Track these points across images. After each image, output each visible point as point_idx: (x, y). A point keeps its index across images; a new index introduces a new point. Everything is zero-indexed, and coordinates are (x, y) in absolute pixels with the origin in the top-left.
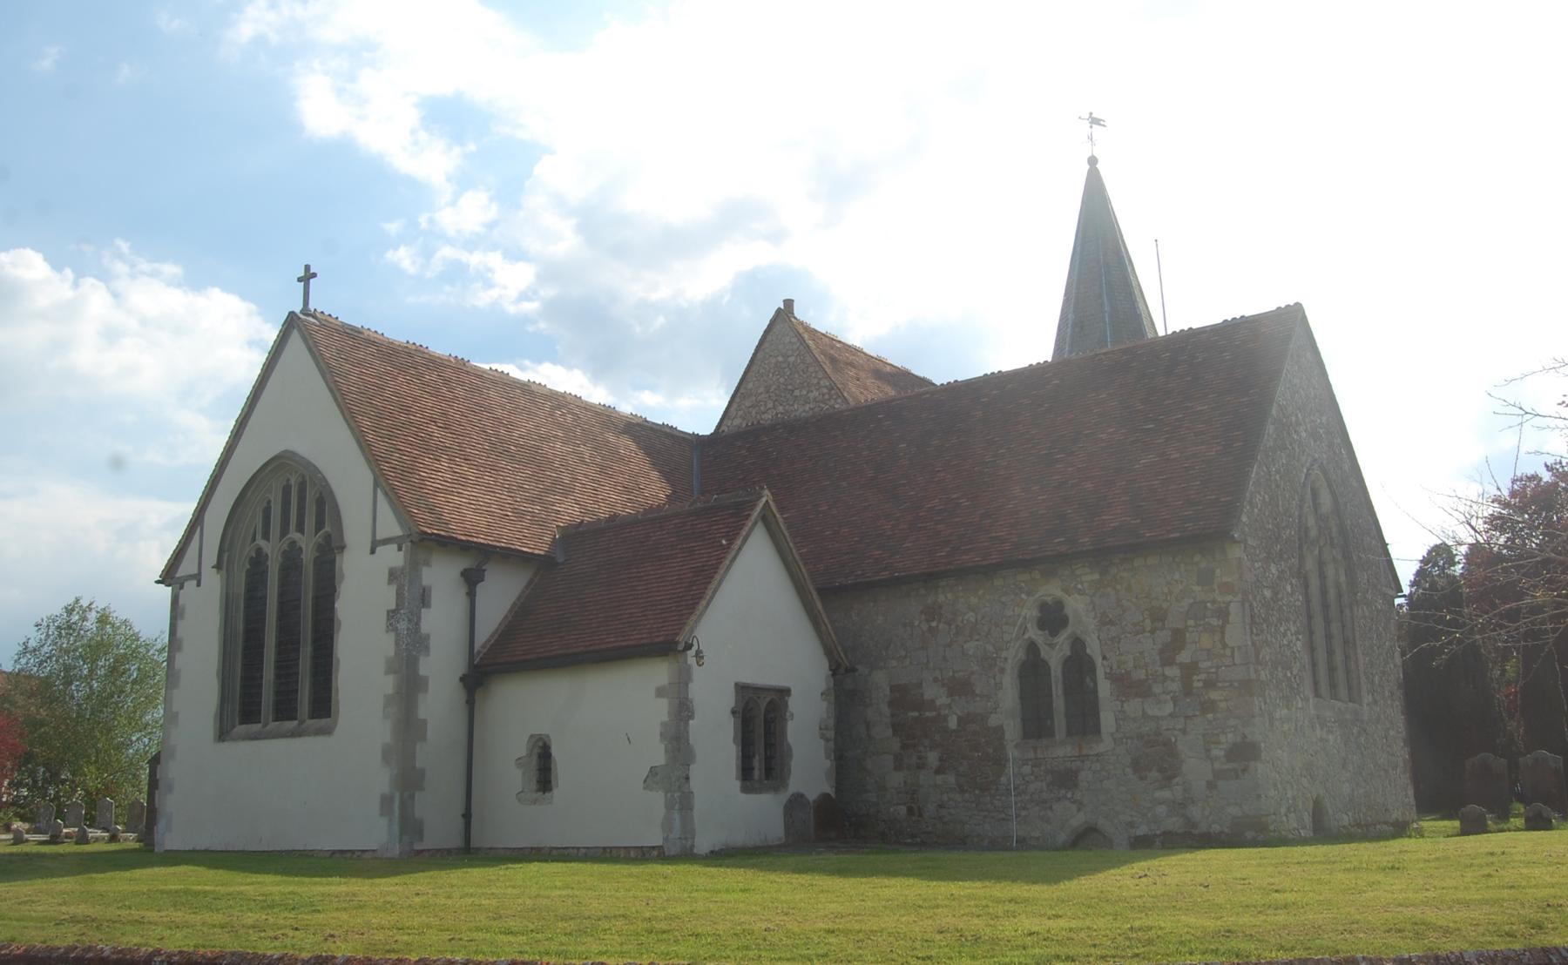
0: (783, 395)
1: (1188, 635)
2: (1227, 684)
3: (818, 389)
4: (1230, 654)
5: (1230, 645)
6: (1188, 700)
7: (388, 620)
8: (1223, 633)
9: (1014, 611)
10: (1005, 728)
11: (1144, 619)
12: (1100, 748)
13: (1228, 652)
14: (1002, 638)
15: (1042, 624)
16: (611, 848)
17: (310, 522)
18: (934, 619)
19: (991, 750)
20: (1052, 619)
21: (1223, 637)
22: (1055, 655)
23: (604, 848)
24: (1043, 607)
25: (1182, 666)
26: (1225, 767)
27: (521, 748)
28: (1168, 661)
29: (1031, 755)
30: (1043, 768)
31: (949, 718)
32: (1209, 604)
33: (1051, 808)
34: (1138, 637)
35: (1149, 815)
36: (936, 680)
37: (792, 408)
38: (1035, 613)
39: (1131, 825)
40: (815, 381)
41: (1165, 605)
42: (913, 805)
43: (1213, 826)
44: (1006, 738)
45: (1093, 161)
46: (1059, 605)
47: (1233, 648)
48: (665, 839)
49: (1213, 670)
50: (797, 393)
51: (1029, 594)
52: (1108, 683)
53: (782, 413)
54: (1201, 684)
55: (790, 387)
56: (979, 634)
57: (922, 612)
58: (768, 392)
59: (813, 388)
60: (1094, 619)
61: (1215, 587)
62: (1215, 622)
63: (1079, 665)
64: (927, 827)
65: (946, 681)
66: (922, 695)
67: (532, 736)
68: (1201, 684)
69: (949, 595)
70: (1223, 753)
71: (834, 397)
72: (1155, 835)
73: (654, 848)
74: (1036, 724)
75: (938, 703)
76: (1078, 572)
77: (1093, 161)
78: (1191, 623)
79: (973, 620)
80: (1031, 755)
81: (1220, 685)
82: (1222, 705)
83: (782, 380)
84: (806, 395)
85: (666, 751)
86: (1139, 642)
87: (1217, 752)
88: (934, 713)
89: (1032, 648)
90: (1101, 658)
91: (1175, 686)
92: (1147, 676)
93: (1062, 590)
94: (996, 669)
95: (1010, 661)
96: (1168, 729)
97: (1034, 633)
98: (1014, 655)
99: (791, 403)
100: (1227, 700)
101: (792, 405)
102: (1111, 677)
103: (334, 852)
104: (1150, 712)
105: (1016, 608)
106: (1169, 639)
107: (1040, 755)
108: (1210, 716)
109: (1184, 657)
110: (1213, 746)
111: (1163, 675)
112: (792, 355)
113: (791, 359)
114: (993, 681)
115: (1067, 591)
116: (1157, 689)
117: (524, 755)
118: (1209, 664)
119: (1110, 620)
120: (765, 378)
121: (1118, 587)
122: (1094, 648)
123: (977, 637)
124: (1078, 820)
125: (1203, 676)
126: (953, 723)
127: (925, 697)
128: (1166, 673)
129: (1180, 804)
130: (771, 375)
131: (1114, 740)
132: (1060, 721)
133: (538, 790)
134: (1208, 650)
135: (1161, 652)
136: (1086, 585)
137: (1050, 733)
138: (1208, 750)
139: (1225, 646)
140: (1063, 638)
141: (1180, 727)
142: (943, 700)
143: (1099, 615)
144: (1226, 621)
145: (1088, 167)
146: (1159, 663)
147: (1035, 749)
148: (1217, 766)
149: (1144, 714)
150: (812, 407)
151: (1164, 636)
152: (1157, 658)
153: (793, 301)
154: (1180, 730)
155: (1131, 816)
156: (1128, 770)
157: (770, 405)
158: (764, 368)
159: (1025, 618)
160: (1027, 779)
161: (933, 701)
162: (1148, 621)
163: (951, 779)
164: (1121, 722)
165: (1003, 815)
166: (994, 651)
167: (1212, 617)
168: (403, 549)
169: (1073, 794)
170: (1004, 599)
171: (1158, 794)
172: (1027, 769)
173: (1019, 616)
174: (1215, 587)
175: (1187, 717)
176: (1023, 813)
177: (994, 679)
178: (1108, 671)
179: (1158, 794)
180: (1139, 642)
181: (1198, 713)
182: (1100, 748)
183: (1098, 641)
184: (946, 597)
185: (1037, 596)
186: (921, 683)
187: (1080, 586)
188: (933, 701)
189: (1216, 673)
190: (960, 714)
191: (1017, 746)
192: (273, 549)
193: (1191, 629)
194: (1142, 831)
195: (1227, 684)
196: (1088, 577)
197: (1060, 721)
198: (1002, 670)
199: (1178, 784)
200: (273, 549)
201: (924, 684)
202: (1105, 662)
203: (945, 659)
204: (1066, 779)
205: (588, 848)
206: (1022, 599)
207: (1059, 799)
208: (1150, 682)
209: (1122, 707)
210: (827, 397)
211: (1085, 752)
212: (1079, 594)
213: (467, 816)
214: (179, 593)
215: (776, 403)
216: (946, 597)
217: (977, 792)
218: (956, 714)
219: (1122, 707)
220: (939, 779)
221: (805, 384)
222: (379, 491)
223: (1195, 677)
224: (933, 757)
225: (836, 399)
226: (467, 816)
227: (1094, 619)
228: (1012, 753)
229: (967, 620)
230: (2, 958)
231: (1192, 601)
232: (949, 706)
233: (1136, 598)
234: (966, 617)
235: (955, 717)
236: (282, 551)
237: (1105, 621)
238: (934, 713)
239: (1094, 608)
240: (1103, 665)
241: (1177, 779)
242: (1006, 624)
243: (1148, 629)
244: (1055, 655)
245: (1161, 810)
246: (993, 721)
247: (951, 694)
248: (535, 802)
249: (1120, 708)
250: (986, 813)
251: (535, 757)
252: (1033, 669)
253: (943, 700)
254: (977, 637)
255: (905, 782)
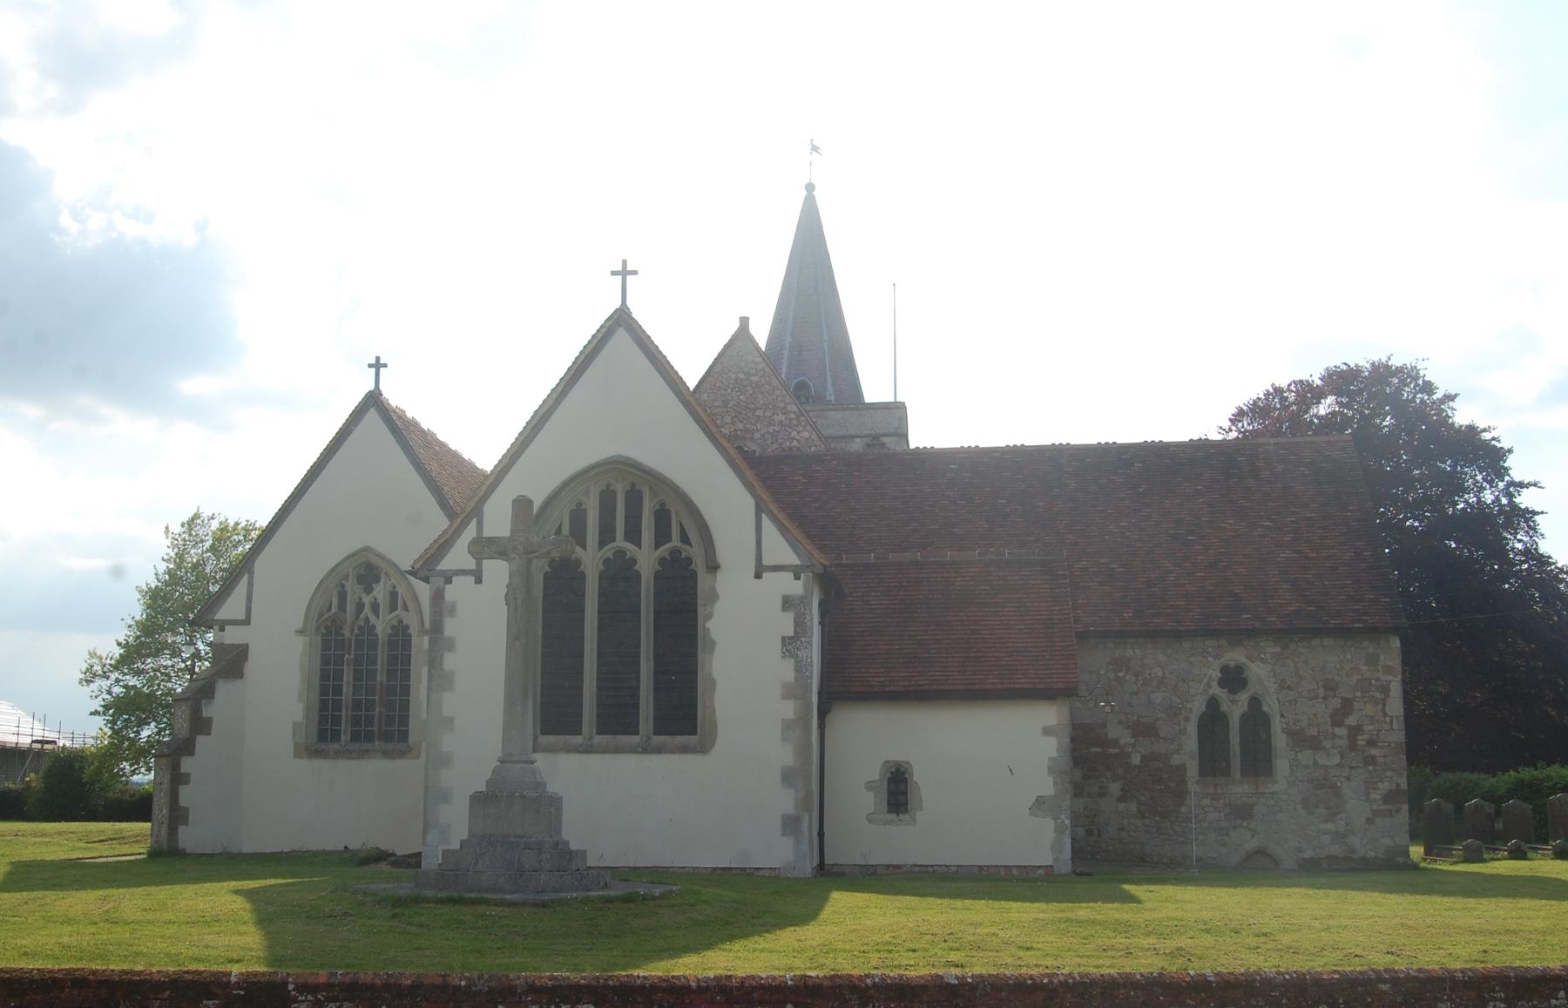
0: (744, 412)
1: (1355, 703)
2: (1386, 744)
3: (785, 413)
4: (1389, 721)
5: (1389, 713)
6: (1353, 754)
7: (784, 645)
8: (1384, 705)
9: (1200, 671)
10: (1187, 766)
11: (1319, 688)
12: (1276, 788)
13: (1388, 720)
14: (1189, 692)
15: (1222, 683)
16: (988, 866)
17: (647, 535)
18: (1121, 671)
19: (1173, 785)
20: (1233, 679)
21: (1384, 708)
22: (1235, 709)
23: (981, 867)
24: (1225, 670)
25: (1350, 728)
26: (1383, 807)
27: (875, 773)
28: (1337, 723)
29: (1211, 790)
30: (1222, 801)
31: (1132, 756)
32: (1373, 681)
33: (1228, 834)
34: (1313, 701)
35: (1315, 842)
36: (1120, 722)
37: (754, 427)
38: (1217, 674)
39: (1299, 850)
40: (782, 405)
41: (1337, 678)
42: (1093, 827)
43: (1369, 852)
44: (1188, 774)
45: (810, 188)
46: (1239, 669)
47: (1392, 717)
48: (1056, 860)
49: (1376, 733)
50: (759, 413)
51: (1215, 658)
52: (1284, 736)
53: (741, 430)
54: (1364, 743)
55: (753, 406)
56: (1166, 687)
57: (1109, 663)
58: (726, 407)
59: (779, 412)
60: (1275, 683)
61: (1380, 668)
62: (1378, 695)
63: (1256, 718)
64: (1108, 846)
65: (1130, 724)
66: (1106, 734)
67: (886, 762)
68: (1364, 743)
69: (1138, 651)
70: (1378, 797)
71: (803, 424)
72: (1320, 858)
73: (1039, 867)
74: (1213, 763)
75: (1122, 741)
76: (1262, 644)
77: (810, 188)
78: (1358, 694)
79: (1160, 674)
80: (1211, 790)
81: (1380, 744)
82: (1381, 760)
83: (742, 397)
84: (771, 417)
85: (1055, 783)
86: (1314, 706)
87: (1375, 796)
88: (1117, 751)
89: (1213, 703)
90: (1279, 716)
91: (1344, 742)
92: (1319, 733)
93: (1247, 658)
94: (1181, 717)
95: (1194, 711)
96: (1334, 776)
97: (1216, 690)
98: (1198, 707)
99: (753, 422)
100: (1384, 756)
101: (755, 425)
102: (1285, 731)
103: (715, 869)
104: (1320, 762)
105: (1203, 669)
106: (1339, 706)
107: (1219, 791)
108: (1371, 768)
109: (1351, 720)
110: (1372, 791)
111: (1333, 732)
112: (756, 375)
113: (755, 379)
114: (1178, 728)
115: (1250, 659)
116: (1327, 744)
117: (878, 778)
118: (1371, 727)
119: (1289, 686)
120: (723, 392)
121: (1296, 660)
122: (1271, 706)
123: (1165, 689)
124: (1252, 844)
125: (1366, 737)
126: (1136, 760)
127: (1110, 736)
128: (1336, 732)
129: (1342, 835)
130: (730, 390)
131: (1288, 782)
132: (1236, 763)
133: (890, 811)
134: (1372, 717)
135: (1332, 715)
136: (1268, 655)
137: (1227, 772)
138: (1368, 794)
139: (1385, 715)
140: (1244, 697)
141: (1345, 775)
142: (1126, 739)
143: (1279, 681)
144: (1387, 696)
145: (805, 193)
146: (1330, 724)
147: (1215, 786)
148: (1374, 807)
149: (1315, 763)
150: (777, 429)
151: (1335, 703)
152: (1329, 720)
153: (748, 318)
154: (1345, 777)
155: (1299, 843)
156: (1299, 806)
157: (728, 420)
158: (722, 382)
159: (1210, 677)
160: (1206, 809)
161: (1117, 740)
162: (1322, 691)
163: (1133, 807)
164: (1295, 768)
165: (1182, 839)
166: (1180, 702)
167: (1376, 691)
168: (802, 578)
169: (1249, 823)
170: (1191, 659)
171: (1322, 826)
172: (1206, 802)
173: (1205, 675)
174: (1380, 668)
175: (1351, 767)
176: (1201, 837)
177: (1179, 726)
178: (1285, 726)
179: (1322, 826)
180: (1314, 706)
181: (1360, 765)
182: (1276, 788)
183: (1277, 702)
184: (1135, 653)
185: (1223, 660)
186: (1106, 724)
187: (1263, 656)
188: (1117, 740)
189: (1377, 735)
190: (1144, 752)
191: (1197, 782)
192: (591, 560)
193: (1357, 699)
194: (1308, 854)
195: (1386, 744)
196: (1271, 649)
197: (1236, 763)
198: (1187, 719)
199: (1341, 819)
200: (591, 560)
201: (1109, 725)
202: (1282, 719)
203: (1130, 705)
204: (1243, 812)
205: (958, 866)
206: (1208, 662)
207: (1235, 827)
208: (1322, 738)
209: (1296, 756)
210: (795, 422)
211: (1261, 790)
212: (1262, 663)
213: (821, 835)
214: (444, 587)
215: (735, 419)
216: (1135, 653)
217: (1157, 818)
218: (1139, 752)
219: (1296, 756)
220: (1121, 807)
221: (771, 407)
222: (765, 520)
223: (1360, 737)
224: (1115, 788)
225: (804, 426)
226: (821, 835)
227: (1275, 683)
228: (1192, 787)
229: (1154, 674)
230: (2, 975)
231: (1359, 677)
232: (1133, 746)
233: (1313, 670)
234: (1154, 671)
235: (1138, 755)
236: (604, 558)
237: (1283, 686)
238: (1117, 751)
239: (1274, 676)
240: (1281, 722)
241: (1341, 815)
242: (1193, 681)
243: (1322, 696)
244: (1235, 709)
245: (1326, 839)
246: (1176, 760)
247: (1134, 736)
248: (887, 823)
249: (1294, 757)
250: (1166, 837)
251: (886, 782)
252: (1213, 719)
253: (1126, 739)
254: (1165, 689)
255: (1085, 808)
